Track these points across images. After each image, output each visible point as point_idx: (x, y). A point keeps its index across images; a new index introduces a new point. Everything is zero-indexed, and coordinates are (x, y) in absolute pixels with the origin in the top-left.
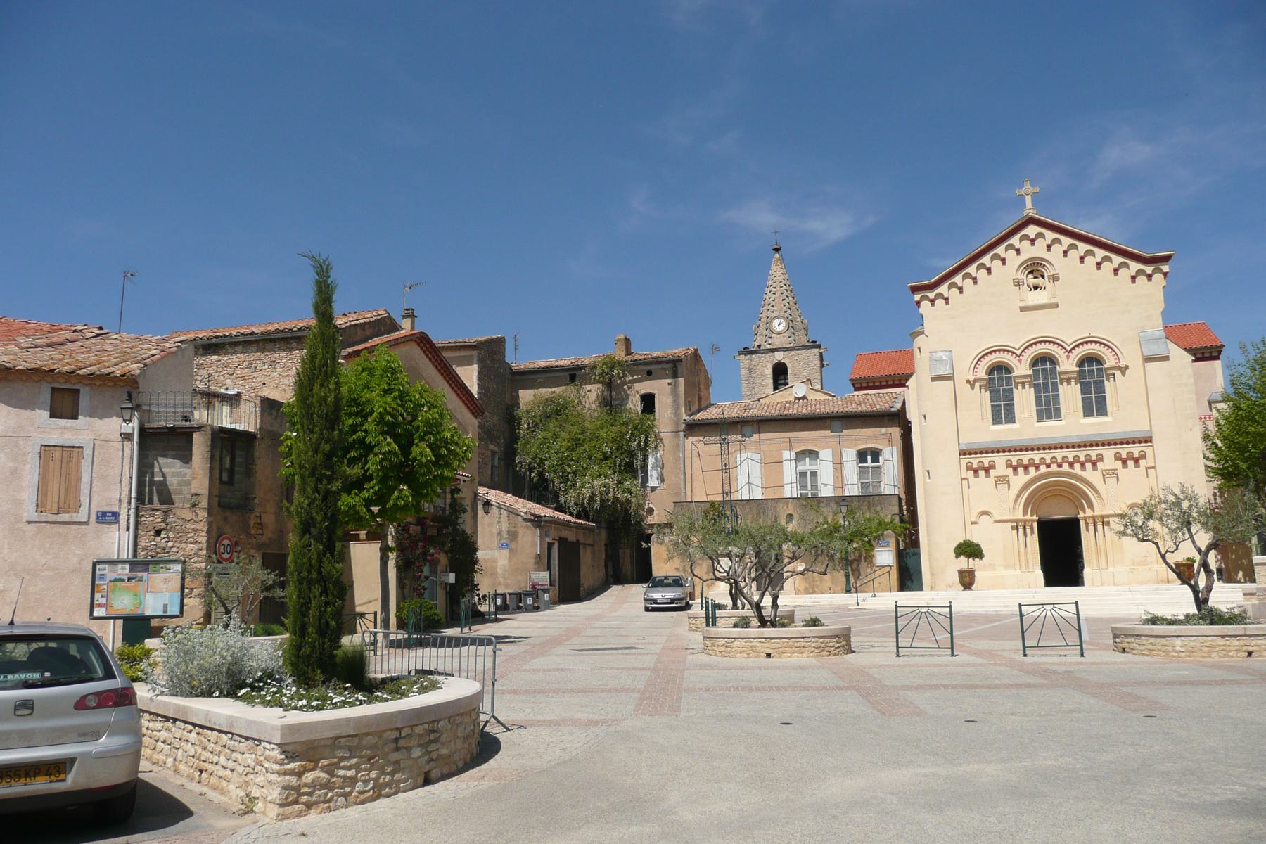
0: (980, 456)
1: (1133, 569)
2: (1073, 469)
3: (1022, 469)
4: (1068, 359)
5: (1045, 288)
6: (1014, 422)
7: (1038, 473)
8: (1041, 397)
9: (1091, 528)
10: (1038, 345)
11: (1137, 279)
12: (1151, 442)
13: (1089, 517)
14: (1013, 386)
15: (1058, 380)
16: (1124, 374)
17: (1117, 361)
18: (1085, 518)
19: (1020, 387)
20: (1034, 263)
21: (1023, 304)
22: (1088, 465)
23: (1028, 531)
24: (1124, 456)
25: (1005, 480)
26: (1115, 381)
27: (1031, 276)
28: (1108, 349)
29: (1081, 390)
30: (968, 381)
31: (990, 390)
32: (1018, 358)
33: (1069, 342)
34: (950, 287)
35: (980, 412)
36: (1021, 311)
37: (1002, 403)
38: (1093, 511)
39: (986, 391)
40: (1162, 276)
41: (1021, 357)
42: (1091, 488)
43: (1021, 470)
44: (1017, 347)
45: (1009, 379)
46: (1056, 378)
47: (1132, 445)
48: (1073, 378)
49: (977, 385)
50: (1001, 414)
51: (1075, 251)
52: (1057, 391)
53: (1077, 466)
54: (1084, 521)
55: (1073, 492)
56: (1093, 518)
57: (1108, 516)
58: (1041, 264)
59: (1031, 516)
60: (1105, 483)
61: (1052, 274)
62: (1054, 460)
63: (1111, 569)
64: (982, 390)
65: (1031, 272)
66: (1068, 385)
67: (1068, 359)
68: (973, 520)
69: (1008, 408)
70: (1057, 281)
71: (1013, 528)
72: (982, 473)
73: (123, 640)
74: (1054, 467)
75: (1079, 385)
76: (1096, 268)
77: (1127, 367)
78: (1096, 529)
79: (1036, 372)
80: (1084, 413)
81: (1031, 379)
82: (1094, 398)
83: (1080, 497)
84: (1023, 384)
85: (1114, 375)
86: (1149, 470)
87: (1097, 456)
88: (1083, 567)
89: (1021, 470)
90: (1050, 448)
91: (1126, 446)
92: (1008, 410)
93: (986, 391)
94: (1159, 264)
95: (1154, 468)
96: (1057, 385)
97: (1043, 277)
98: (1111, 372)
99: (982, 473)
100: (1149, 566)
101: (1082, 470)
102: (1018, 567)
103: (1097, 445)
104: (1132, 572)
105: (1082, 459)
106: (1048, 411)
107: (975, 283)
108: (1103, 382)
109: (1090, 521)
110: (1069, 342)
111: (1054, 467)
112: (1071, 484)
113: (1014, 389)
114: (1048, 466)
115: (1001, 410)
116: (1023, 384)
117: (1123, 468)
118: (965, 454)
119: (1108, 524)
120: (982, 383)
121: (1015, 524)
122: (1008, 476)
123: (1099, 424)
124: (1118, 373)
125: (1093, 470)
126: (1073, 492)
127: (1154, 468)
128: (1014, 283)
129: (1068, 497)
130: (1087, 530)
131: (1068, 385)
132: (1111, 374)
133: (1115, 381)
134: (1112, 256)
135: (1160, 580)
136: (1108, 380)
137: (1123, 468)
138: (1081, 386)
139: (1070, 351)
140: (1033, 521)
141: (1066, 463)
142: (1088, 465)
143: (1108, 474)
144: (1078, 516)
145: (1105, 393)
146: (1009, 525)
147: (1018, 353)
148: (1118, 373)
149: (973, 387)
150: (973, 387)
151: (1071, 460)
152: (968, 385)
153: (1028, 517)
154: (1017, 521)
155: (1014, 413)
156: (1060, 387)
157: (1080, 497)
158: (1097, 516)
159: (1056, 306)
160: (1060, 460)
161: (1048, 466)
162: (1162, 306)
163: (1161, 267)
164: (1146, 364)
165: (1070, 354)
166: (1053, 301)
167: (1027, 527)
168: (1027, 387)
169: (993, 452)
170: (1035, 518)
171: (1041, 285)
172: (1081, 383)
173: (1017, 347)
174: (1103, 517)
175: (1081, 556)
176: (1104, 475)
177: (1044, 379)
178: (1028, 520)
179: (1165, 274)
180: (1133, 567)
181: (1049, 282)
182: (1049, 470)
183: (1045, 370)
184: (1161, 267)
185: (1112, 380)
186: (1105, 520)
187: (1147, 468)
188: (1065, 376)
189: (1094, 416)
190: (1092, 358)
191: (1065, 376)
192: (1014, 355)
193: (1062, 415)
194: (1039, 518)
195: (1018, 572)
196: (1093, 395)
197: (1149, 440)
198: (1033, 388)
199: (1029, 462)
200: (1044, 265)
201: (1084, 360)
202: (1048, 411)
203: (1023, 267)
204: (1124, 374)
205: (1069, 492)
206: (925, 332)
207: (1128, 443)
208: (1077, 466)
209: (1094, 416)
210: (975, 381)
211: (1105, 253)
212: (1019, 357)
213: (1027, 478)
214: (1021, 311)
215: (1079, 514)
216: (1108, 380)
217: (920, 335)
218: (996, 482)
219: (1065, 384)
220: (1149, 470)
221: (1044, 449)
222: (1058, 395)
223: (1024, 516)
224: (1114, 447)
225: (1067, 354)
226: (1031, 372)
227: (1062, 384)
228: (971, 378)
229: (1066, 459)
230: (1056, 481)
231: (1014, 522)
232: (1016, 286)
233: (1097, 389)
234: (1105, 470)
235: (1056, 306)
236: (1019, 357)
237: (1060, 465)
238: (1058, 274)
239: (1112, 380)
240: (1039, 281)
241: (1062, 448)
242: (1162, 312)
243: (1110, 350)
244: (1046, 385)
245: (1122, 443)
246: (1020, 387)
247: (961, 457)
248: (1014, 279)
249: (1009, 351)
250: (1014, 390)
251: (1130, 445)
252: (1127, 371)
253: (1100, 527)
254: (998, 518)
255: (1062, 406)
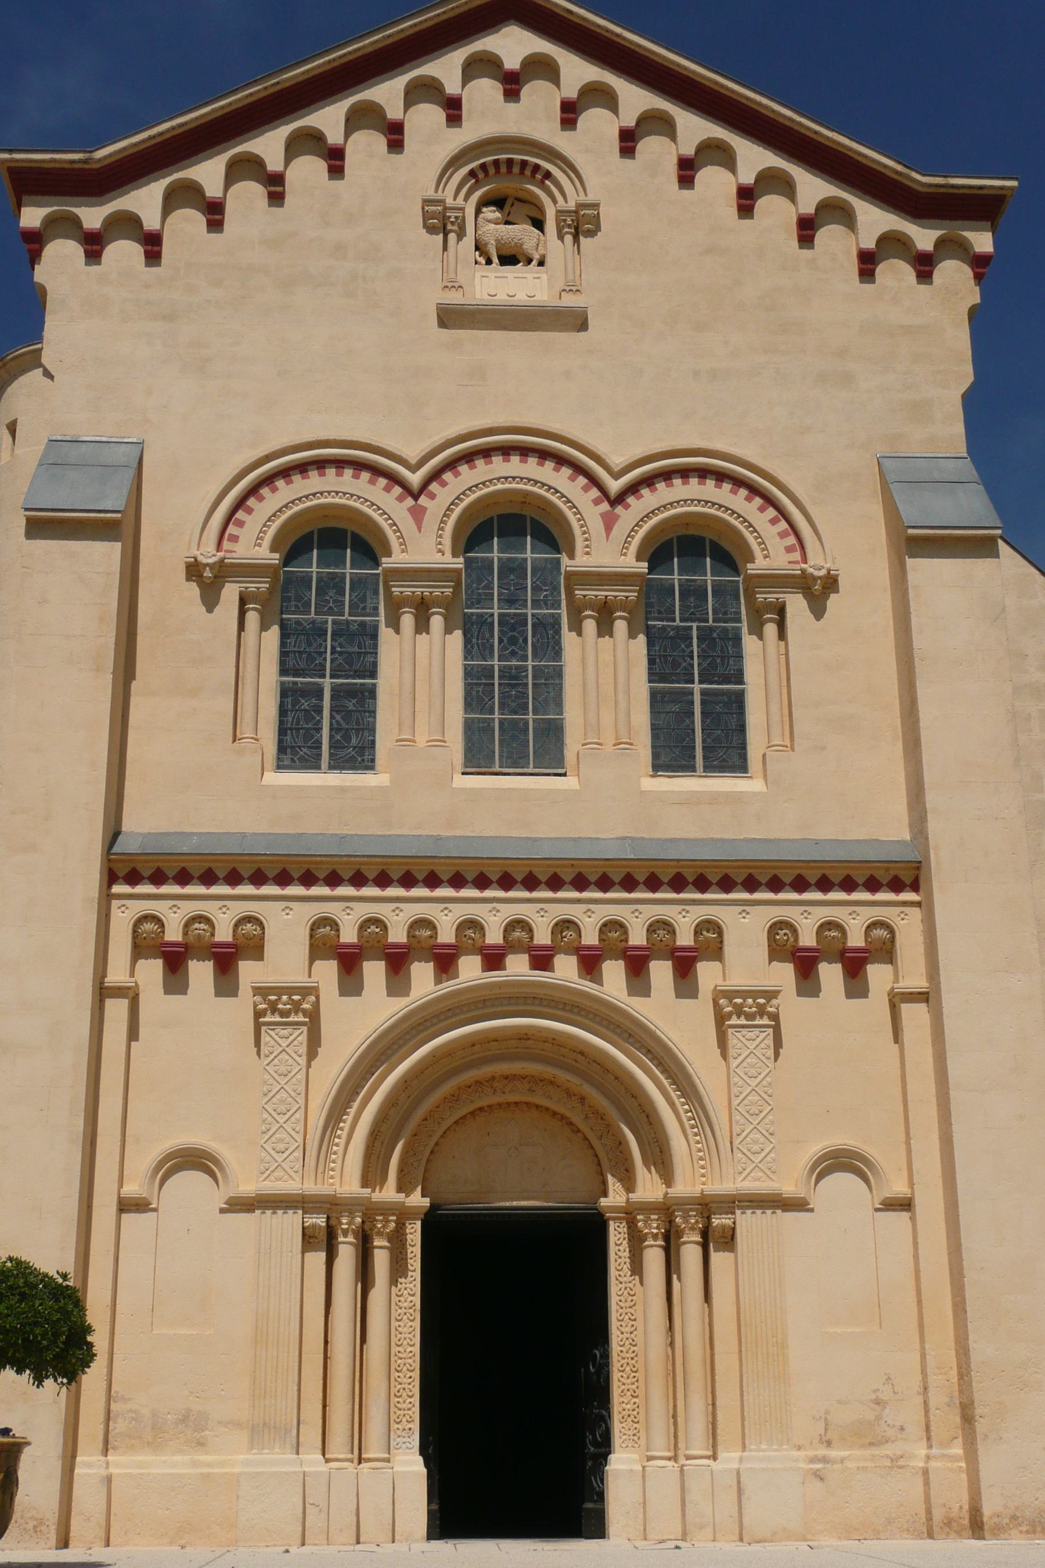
0: (201, 890)
1: (825, 1460)
2: (600, 983)
3: (667, 965)
4: (608, 528)
5: (541, 263)
6: (371, 768)
7: (449, 986)
8: (489, 672)
9: (654, 1258)
10: (497, 459)
11: (880, 269)
12: (915, 887)
13: (648, 1208)
14: (382, 618)
15: (564, 612)
16: (818, 610)
17: (797, 556)
18: (630, 1214)
19: (407, 621)
20: (510, 162)
21: (454, 298)
22: (661, 972)
23: (381, 1260)
24: (808, 939)
25: (297, 1008)
26: (782, 635)
27: (491, 213)
28: (762, 509)
29: (651, 661)
30: (194, 570)
31: (283, 627)
32: (410, 502)
33: (617, 461)
34: (172, 200)
35: (980, 1348)
36: (443, 323)
37: (327, 683)
38: (667, 1176)
39: (264, 627)
40: (967, 272)
41: (423, 500)
42: (660, 1064)
43: (374, 971)
44: (413, 457)
45: (364, 587)
46: (557, 605)
47: (842, 896)
48: (624, 605)
49: (230, 592)
50: (319, 730)
51: (665, 140)
52: (558, 654)
53: (614, 971)
54: (623, 1228)
55: (588, 1090)
56: (666, 1210)
57: (733, 1203)
58: (537, 168)
59: (400, 1190)
60: (724, 1055)
61: (571, 205)
62: (517, 934)
63: (729, 1459)
64: (252, 618)
65: (499, 202)
66: (600, 634)
67: (608, 528)
68: (132, 1189)
69: (351, 704)
70: (591, 233)
71: (308, 1239)
72: (830, 974)
73: (545, 970)
74: (517, 966)
75: (642, 638)
76: (734, 210)
77: (831, 583)
78: (671, 1266)
79: (477, 570)
80: (655, 756)
81: (457, 587)
82: (697, 699)
83: (612, 1113)
84: (422, 609)
85: (781, 611)
86: (905, 1008)
87: (697, 932)
88: (605, 1446)
89: (374, 971)
90: (506, 882)
91: (818, 896)
92: (348, 715)
93: (264, 627)
94: (959, 223)
95: (922, 997)
96: (558, 632)
97: (539, 224)
98: (772, 597)
99: (830, 974)
100: (889, 1450)
101: (632, 991)
102: (312, 1434)
103: (702, 884)
104: (818, 1476)
105: (638, 938)
106: (514, 732)
107: (276, 198)
108: (737, 640)
109: (652, 1226)
110: (617, 461)
111: (517, 966)
112: (583, 1051)
113: (382, 627)
114: (493, 960)
115: (319, 710)
116: (422, 609)
117: (801, 992)
118: (133, 878)
119: (728, 1240)
120: (252, 587)
121: (321, 1221)
122: (313, 991)
123: (714, 798)
124: (796, 605)
125: (680, 994)
126: (588, 1090)
127: (922, 997)
128: (426, 216)
129: (563, 1117)
130: (637, 1267)
131: (600, 634)
132: (769, 607)
133: (782, 635)
134: (801, 176)
135: (938, 1515)
136: (757, 631)
137: (801, 992)
138: (650, 644)
139: (619, 500)
140: (403, 1215)
141: (567, 953)
142: (661, 972)
143: (739, 1011)
144: (604, 1202)
145: (741, 682)
146: (292, 1223)
147: (415, 479)
148: (796, 605)
149: (210, 599)
150: (210, 599)
151: (590, 938)
152: (193, 590)
153: (388, 1193)
154: (331, 1206)
155: (373, 730)
156: (568, 638)
157: (612, 1113)
158: (683, 1203)
159: (578, 322)
160: (543, 937)
161: (493, 960)
162: (965, 374)
163: (966, 234)
164: (910, 562)
165: (619, 510)
166: (569, 301)
167: (378, 1242)
168: (437, 622)
169: (259, 878)
170: (418, 1200)
171: (529, 246)
172: (649, 632)
173: (413, 457)
174: (706, 1206)
175: (601, 1393)
176: (721, 1019)
177: (509, 601)
178: (385, 1209)
179: (979, 263)
180: (822, 1452)
181: (561, 237)
182: (495, 976)
183: (512, 570)
184: (966, 234)
185: (770, 630)
186: (718, 1221)
187: (896, 1000)
188: (591, 593)
189: (693, 769)
190: (702, 540)
191: (591, 593)
192: (397, 490)
193: (570, 755)
194: (434, 1207)
195: (312, 1461)
196: (697, 687)
197: (907, 878)
198: (458, 635)
199: (410, 935)
200: (548, 175)
201: (670, 542)
202: (514, 732)
203: (465, 170)
204: (818, 610)
205: (569, 1094)
206: (45, 360)
207: (824, 885)
208: (614, 971)
209: (693, 769)
210: (224, 572)
211: (770, 159)
212: (416, 497)
213: (397, 1007)
214: (443, 323)
215: (605, 1194)
216: (757, 631)
217: (24, 371)
218: (258, 1014)
219: (590, 626)
220: (905, 1008)
221: (482, 882)
222: (559, 673)
223: (365, 1183)
224: (770, 896)
225: (605, 506)
226: (459, 563)
227: (577, 627)
228: (208, 554)
229: (570, 935)
230: (524, 1036)
231: (317, 1211)
232: (431, 230)
233: (713, 665)
234: (730, 995)
235: (578, 322)
236: (416, 497)
237: (542, 960)
238: (596, 206)
239: (770, 630)
240: (522, 233)
241: (555, 883)
242: (964, 397)
243: (771, 512)
244: (513, 626)
245: (800, 885)
246: (407, 621)
247: (117, 889)
248: (427, 202)
249: (377, 471)
250: (385, 633)
251: (881, 896)
252: (833, 601)
253: (690, 1254)
254: (248, 1187)
255: (572, 716)
